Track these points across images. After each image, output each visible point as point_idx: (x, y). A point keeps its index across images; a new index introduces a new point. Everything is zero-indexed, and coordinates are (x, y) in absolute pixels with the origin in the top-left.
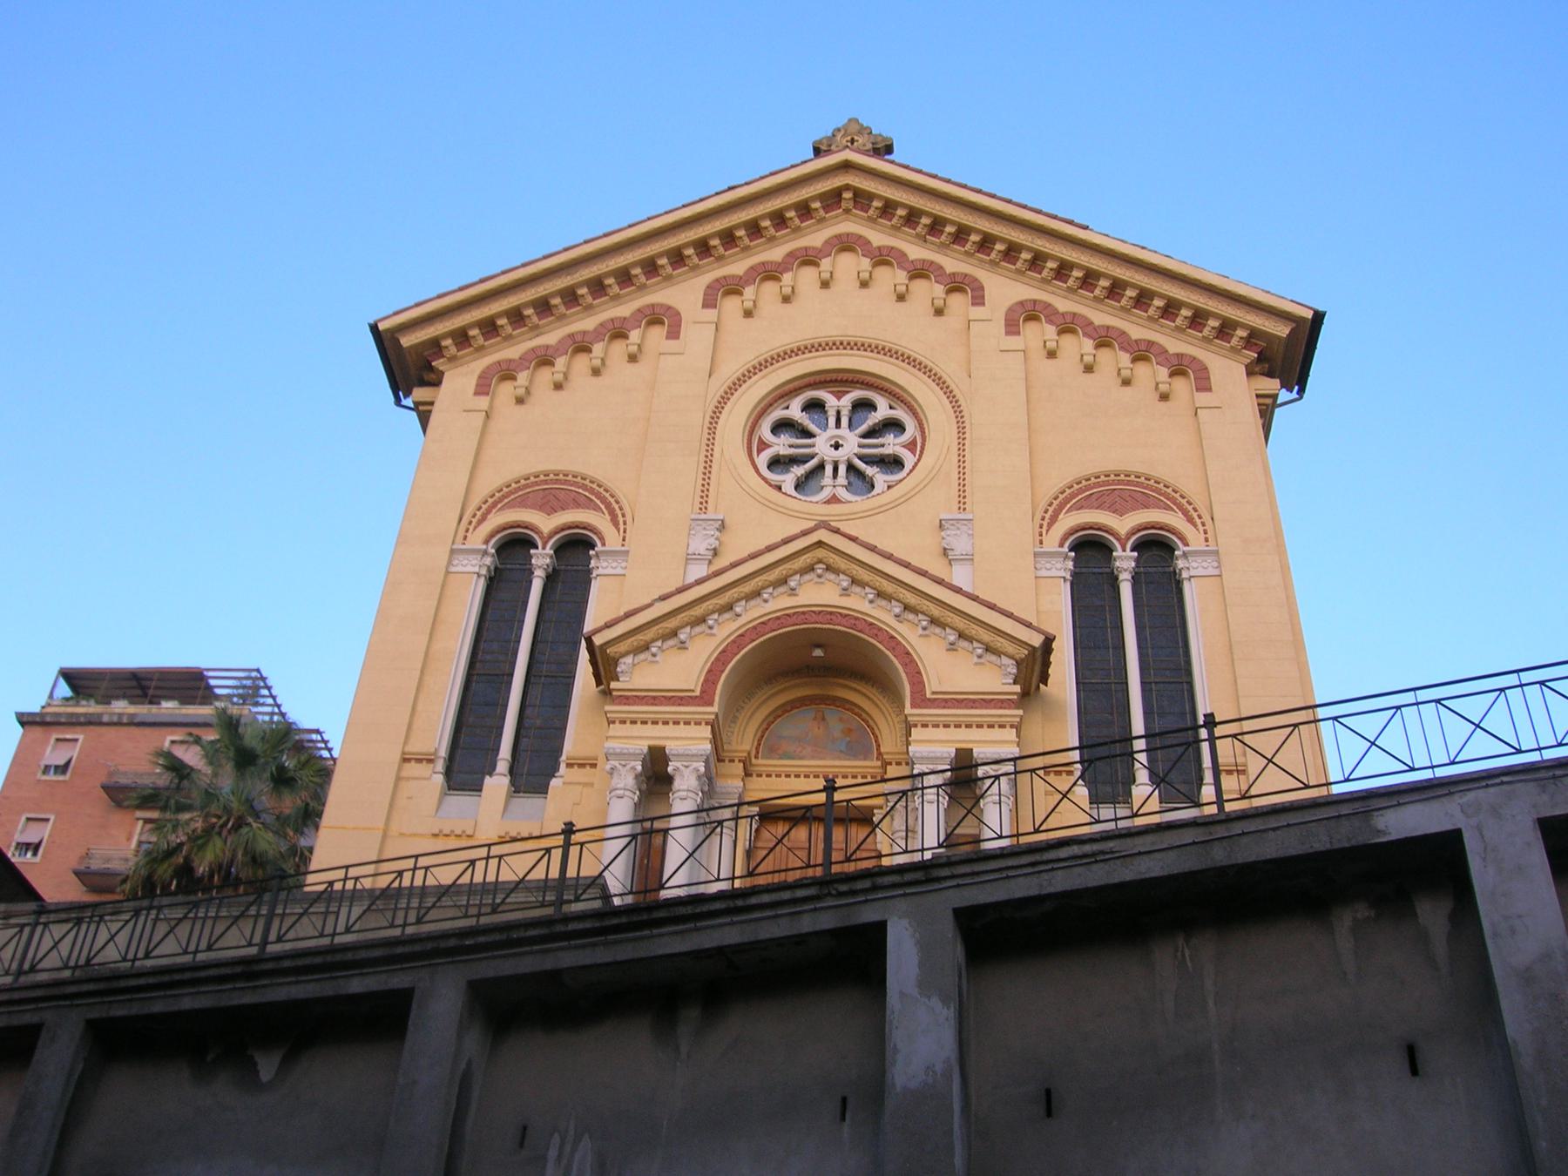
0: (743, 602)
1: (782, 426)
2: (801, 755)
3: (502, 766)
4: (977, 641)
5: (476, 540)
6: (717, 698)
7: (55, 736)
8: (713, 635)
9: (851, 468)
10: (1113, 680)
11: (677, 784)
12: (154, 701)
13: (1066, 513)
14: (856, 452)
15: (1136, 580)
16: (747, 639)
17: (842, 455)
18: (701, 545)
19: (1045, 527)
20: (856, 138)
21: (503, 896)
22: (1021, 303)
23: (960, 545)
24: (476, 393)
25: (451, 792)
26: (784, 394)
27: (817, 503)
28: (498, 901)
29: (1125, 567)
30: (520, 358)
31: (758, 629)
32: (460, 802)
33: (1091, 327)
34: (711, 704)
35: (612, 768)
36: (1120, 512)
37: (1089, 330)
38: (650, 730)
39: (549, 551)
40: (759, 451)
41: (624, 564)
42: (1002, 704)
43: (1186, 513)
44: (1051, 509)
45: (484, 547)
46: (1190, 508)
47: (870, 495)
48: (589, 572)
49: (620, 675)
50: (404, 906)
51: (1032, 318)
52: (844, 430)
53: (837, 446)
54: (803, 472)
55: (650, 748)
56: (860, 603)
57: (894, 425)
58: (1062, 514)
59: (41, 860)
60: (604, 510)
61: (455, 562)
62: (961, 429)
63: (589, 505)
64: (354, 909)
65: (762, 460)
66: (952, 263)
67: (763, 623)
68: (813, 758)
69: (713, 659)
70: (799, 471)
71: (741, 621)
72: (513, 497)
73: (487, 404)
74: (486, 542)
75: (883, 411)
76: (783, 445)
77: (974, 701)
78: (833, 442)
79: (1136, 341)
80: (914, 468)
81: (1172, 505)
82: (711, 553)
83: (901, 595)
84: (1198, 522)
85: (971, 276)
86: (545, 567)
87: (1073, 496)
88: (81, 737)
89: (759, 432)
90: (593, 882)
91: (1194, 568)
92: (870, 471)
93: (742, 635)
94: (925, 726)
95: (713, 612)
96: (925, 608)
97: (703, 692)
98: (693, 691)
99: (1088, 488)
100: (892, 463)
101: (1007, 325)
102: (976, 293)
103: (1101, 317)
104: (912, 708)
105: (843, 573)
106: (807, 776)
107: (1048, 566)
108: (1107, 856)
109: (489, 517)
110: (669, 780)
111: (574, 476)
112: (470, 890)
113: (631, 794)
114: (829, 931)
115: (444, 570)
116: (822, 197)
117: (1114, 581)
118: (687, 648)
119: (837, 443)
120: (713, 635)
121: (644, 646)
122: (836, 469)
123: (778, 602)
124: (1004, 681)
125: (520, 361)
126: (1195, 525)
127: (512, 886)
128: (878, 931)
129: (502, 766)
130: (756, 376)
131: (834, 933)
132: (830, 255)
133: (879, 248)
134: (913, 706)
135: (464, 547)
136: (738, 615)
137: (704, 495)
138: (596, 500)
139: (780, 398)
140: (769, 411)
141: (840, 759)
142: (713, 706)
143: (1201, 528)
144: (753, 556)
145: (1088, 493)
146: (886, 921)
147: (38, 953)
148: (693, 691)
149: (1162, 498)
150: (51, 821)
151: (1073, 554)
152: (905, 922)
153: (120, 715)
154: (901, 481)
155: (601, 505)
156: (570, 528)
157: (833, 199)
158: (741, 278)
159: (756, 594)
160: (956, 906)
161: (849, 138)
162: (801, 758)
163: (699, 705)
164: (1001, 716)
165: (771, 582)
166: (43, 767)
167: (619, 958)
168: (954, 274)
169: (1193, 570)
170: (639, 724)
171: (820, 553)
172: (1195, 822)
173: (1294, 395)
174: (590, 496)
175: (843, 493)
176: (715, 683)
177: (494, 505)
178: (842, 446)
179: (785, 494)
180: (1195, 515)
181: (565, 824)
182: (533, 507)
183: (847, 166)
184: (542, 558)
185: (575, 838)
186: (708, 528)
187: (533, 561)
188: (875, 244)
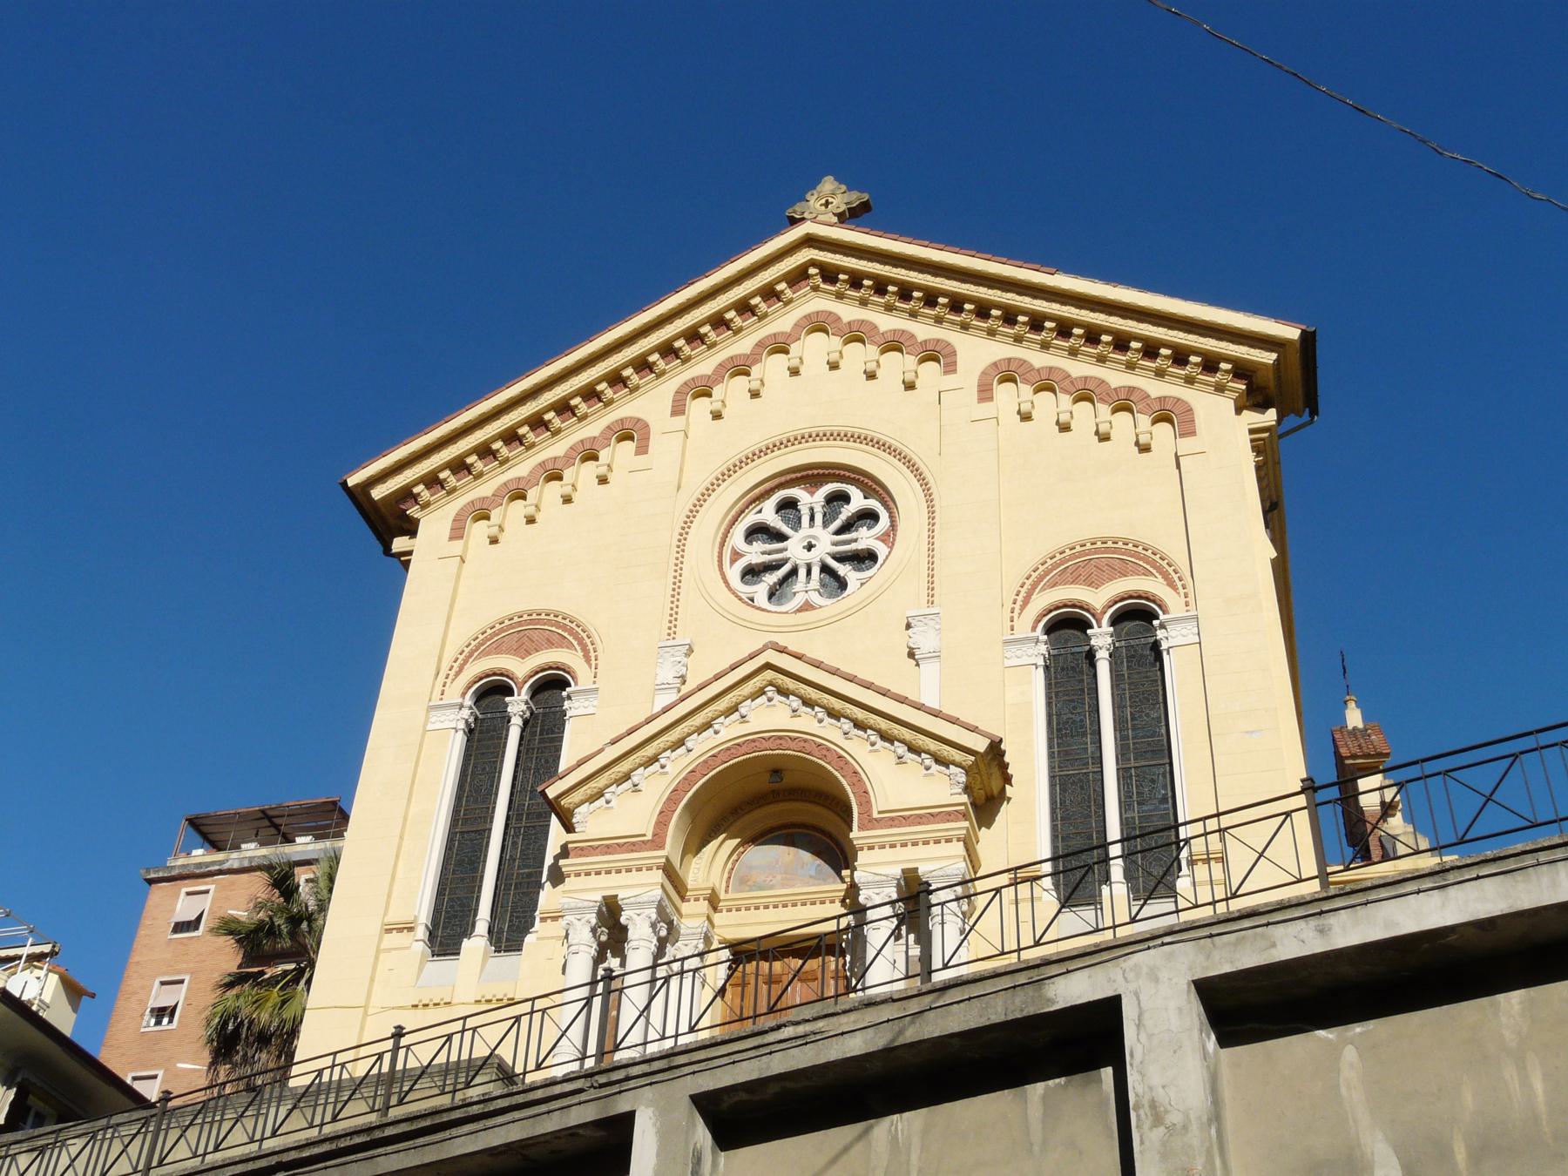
1: (759, 531)
3: (482, 926)
4: (925, 753)
5: (454, 693)
6: (669, 840)
7: (184, 890)
8: (666, 773)
9: (825, 569)
10: (1091, 769)
11: (630, 935)
12: (289, 840)
13: (1039, 592)
14: (828, 551)
15: (1114, 656)
16: (698, 774)
17: (815, 556)
18: (667, 674)
19: (1017, 611)
20: (830, 200)
21: (411, 1083)
22: (995, 364)
23: (924, 640)
24: (451, 538)
25: (435, 958)
26: (758, 497)
27: (787, 613)
28: (406, 1088)
29: (1101, 645)
30: (493, 495)
31: (709, 763)
32: (445, 965)
33: (1067, 382)
34: (662, 847)
35: (568, 924)
36: (1093, 583)
37: (1066, 383)
38: (604, 880)
40: (733, 562)
41: (595, 703)
42: (949, 817)
43: (1166, 576)
44: (1024, 590)
45: (460, 700)
46: (1170, 570)
47: (844, 595)
48: (564, 713)
49: (576, 825)
50: (323, 1101)
51: (1009, 379)
52: (818, 529)
54: (776, 580)
55: (604, 898)
56: (809, 723)
57: (869, 516)
59: (178, 1026)
60: (577, 646)
61: (433, 720)
63: (561, 642)
64: (281, 1109)
66: (923, 330)
67: (714, 756)
68: (783, 886)
70: (771, 578)
71: (693, 755)
72: (489, 643)
73: (461, 548)
74: (464, 694)
75: (858, 501)
76: (756, 553)
77: (920, 816)
78: (806, 544)
79: (1115, 389)
80: (887, 557)
81: (1151, 569)
82: (679, 680)
83: (849, 711)
84: (1179, 584)
85: (943, 341)
86: (521, 713)
87: (1047, 572)
88: (212, 887)
89: (732, 542)
90: (484, 1063)
91: (1173, 638)
92: (843, 569)
94: (871, 848)
95: (665, 750)
96: (872, 722)
97: (654, 835)
98: (644, 835)
99: (1062, 562)
100: (864, 559)
101: (980, 391)
102: (949, 360)
103: (1080, 368)
104: (859, 831)
105: (792, 694)
106: (776, 907)
108: (818, 1037)
109: (466, 667)
110: (625, 929)
111: (547, 615)
112: (378, 1081)
113: (588, 949)
114: (591, 1122)
115: (421, 729)
117: (1091, 656)
119: (810, 543)
120: (666, 773)
121: (598, 793)
122: (809, 573)
123: (729, 730)
124: (953, 791)
126: (1175, 588)
127: (418, 1073)
128: (628, 1119)
129: (482, 926)
131: (597, 1124)
132: (799, 339)
133: (849, 323)
134: (861, 828)
135: (441, 703)
136: (689, 751)
137: (672, 619)
138: (568, 637)
139: (751, 504)
140: (740, 519)
142: (664, 849)
143: (1182, 591)
144: (717, 677)
145: (1063, 567)
146: (635, 1111)
147: (88, 1152)
148: (644, 835)
149: (1141, 563)
150: (186, 982)
152: (650, 1111)
153: (251, 859)
154: (871, 578)
155: (573, 641)
156: (1058, 608)
157: (798, 277)
158: (709, 377)
159: (708, 725)
160: (692, 1093)
161: (823, 201)
162: (771, 888)
163: (651, 850)
164: (947, 830)
166: (172, 925)
167: (427, 1160)
168: (925, 341)
169: (1173, 636)
171: (769, 675)
172: (891, 998)
173: (1306, 417)
174: (563, 633)
175: (815, 598)
176: (666, 825)
177: (1034, 587)
179: (759, 608)
180: (1175, 577)
181: (395, 1028)
183: (810, 241)
184: (517, 705)
185: (404, 1041)
186: (676, 654)
187: (509, 709)
188: (846, 319)
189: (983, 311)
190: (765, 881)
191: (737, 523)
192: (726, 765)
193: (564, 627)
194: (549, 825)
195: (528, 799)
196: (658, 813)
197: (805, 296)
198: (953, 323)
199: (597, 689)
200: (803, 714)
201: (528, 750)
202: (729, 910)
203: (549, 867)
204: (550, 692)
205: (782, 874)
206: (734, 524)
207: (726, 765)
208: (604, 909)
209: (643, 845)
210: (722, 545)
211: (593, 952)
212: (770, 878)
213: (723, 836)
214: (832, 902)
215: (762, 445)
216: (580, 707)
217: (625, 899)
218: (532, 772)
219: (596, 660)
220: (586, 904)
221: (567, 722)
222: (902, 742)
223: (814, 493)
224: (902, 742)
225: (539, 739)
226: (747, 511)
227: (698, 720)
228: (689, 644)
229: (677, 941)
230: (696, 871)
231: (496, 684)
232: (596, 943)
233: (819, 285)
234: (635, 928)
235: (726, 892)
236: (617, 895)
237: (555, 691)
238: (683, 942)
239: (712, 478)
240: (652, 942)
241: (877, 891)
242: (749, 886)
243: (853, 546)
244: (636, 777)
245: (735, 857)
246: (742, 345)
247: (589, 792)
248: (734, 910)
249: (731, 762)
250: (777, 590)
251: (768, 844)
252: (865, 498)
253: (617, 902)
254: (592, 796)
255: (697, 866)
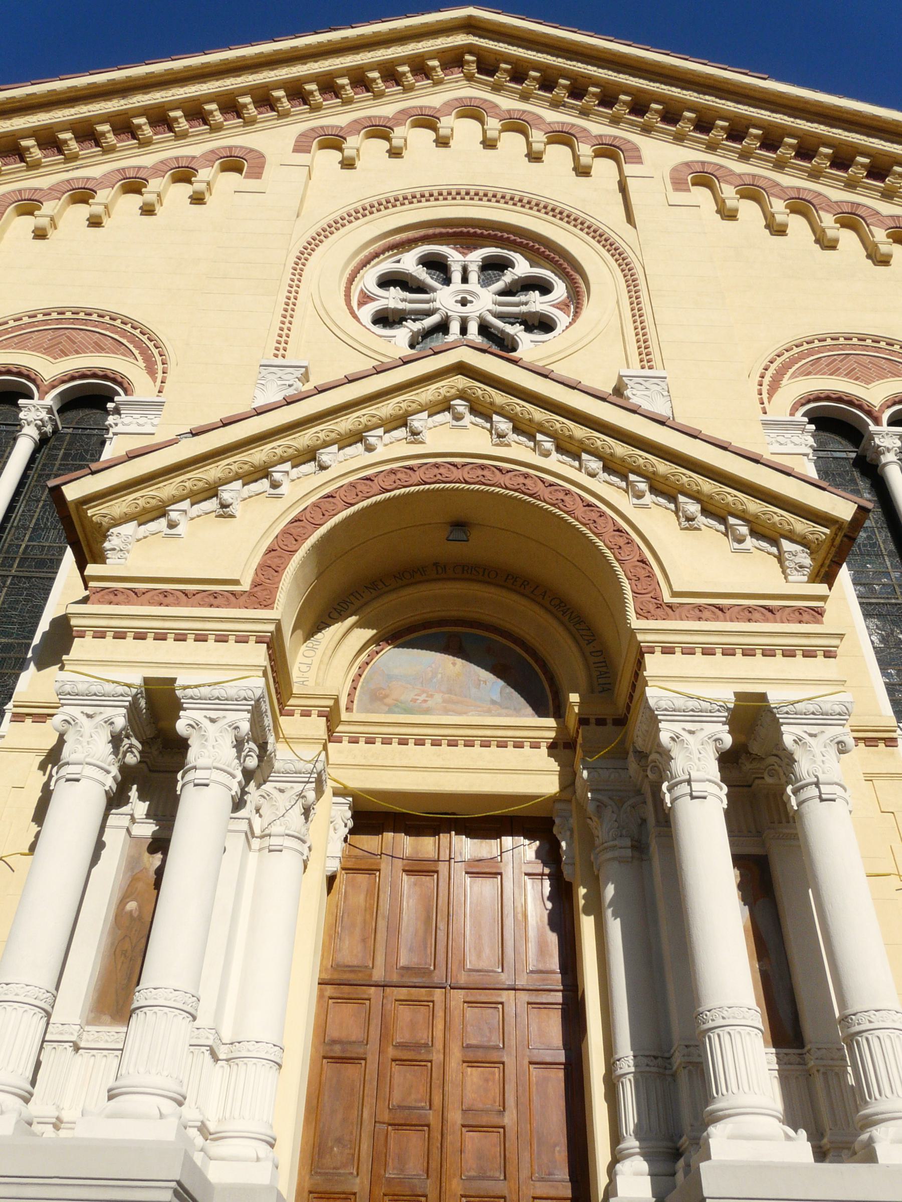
0: (335, 448)
1: (386, 282)
2: (425, 705)
8: (279, 496)
9: (485, 329)
11: (193, 756)
17: (474, 311)
25: (586, 717)
30: (49, 189)
38: (149, 649)
39: (50, 399)
41: (156, 421)
49: (109, 554)
53: (464, 302)
55: (147, 681)
58: (787, 377)
60: (138, 356)
62: (631, 282)
65: (367, 313)
69: (277, 531)
75: (522, 267)
78: (459, 298)
86: (39, 423)
93: (330, 496)
94: (668, 651)
95: (283, 461)
97: (255, 584)
106: (436, 743)
107: (780, 439)
110: (181, 746)
111: (100, 316)
116: (439, 54)
118: (232, 516)
125: (49, 191)
130: (359, 221)
132: (450, 115)
140: (373, 263)
141: (489, 712)
148: (236, 582)
151: (813, 427)
162: (427, 711)
165: (381, 419)
170: (130, 639)
171: (461, 382)
178: (471, 302)
182: (36, 348)
186: (284, 377)
189: (671, 116)
190: (415, 701)
191: (368, 266)
192: (388, 495)
193: (124, 333)
194: (54, 579)
195: (27, 538)
196: (264, 549)
197: (457, 82)
198: (632, 124)
199: (162, 404)
200: (513, 444)
201: (40, 476)
202: (354, 741)
203: (44, 633)
204: (87, 411)
205: (443, 692)
206: (365, 266)
207: (388, 495)
208: (143, 703)
209: (232, 598)
210: (351, 281)
211: (110, 783)
212: (423, 697)
213: (352, 619)
214: (535, 746)
215: (408, 193)
216: (131, 423)
217: (188, 687)
218: (41, 504)
219: (162, 382)
220: (109, 688)
221: (108, 443)
222: (696, 497)
223: (466, 254)
224: (696, 497)
225: (60, 465)
226: (382, 257)
227: (345, 424)
228: (306, 367)
229: (265, 782)
230: (304, 668)
231: (9, 389)
232: (117, 765)
233: (474, 74)
234: (203, 746)
235: (348, 709)
236: (175, 679)
237: (94, 411)
238: (278, 785)
239: (343, 212)
240: (234, 777)
241: (690, 726)
242: (388, 705)
243: (524, 309)
244: (228, 493)
245: (364, 657)
246: (386, 110)
247: (141, 502)
248: (362, 741)
249: (397, 492)
250: (418, 344)
251: (403, 647)
252: (531, 267)
253: (174, 690)
254: (145, 511)
255: (308, 661)
